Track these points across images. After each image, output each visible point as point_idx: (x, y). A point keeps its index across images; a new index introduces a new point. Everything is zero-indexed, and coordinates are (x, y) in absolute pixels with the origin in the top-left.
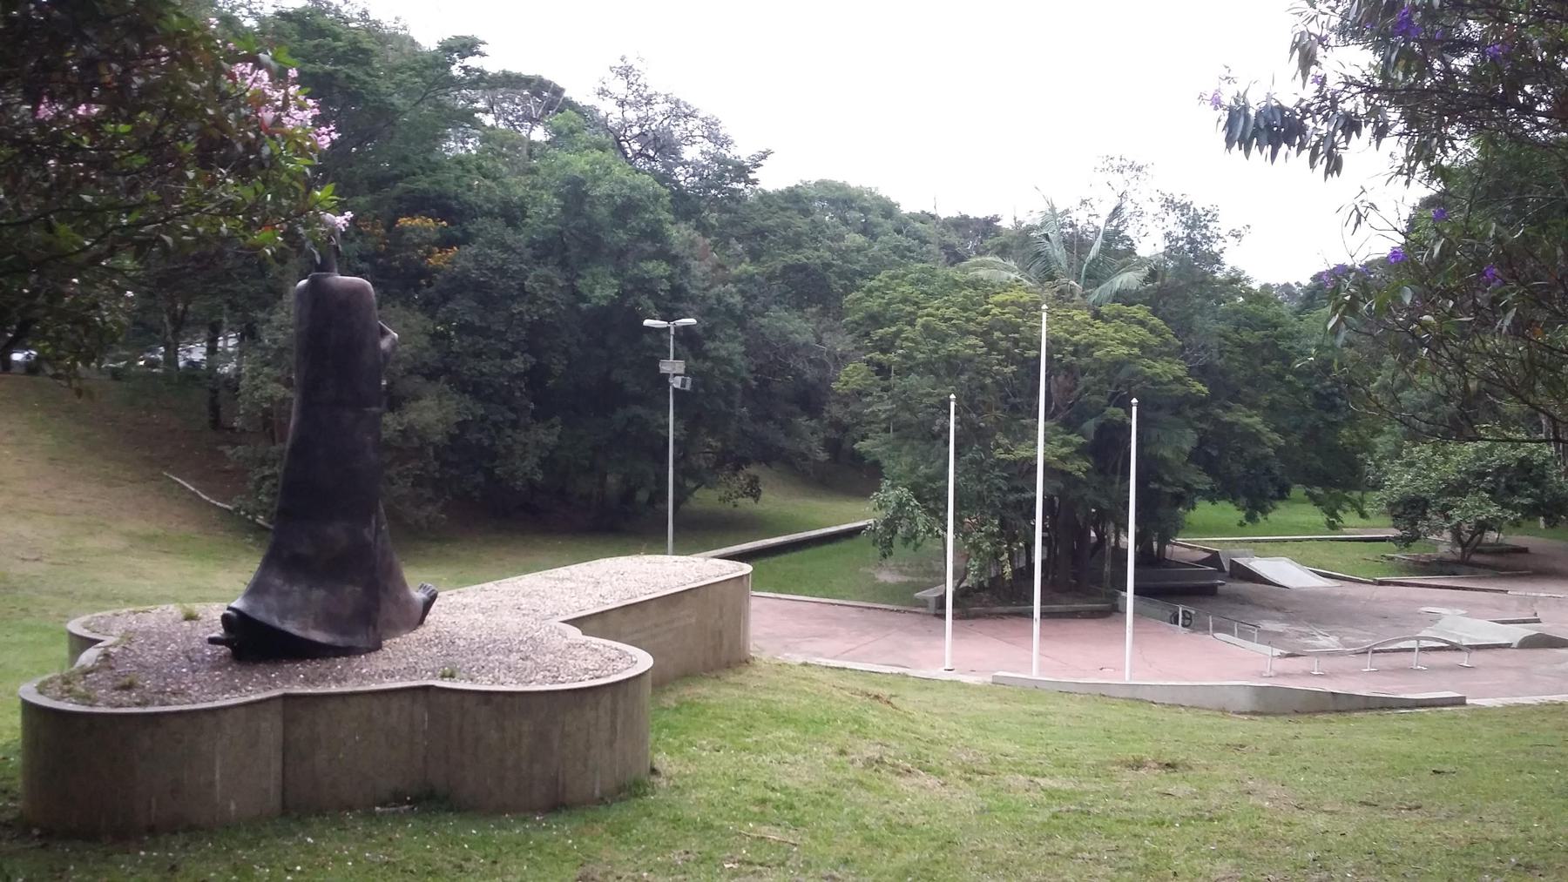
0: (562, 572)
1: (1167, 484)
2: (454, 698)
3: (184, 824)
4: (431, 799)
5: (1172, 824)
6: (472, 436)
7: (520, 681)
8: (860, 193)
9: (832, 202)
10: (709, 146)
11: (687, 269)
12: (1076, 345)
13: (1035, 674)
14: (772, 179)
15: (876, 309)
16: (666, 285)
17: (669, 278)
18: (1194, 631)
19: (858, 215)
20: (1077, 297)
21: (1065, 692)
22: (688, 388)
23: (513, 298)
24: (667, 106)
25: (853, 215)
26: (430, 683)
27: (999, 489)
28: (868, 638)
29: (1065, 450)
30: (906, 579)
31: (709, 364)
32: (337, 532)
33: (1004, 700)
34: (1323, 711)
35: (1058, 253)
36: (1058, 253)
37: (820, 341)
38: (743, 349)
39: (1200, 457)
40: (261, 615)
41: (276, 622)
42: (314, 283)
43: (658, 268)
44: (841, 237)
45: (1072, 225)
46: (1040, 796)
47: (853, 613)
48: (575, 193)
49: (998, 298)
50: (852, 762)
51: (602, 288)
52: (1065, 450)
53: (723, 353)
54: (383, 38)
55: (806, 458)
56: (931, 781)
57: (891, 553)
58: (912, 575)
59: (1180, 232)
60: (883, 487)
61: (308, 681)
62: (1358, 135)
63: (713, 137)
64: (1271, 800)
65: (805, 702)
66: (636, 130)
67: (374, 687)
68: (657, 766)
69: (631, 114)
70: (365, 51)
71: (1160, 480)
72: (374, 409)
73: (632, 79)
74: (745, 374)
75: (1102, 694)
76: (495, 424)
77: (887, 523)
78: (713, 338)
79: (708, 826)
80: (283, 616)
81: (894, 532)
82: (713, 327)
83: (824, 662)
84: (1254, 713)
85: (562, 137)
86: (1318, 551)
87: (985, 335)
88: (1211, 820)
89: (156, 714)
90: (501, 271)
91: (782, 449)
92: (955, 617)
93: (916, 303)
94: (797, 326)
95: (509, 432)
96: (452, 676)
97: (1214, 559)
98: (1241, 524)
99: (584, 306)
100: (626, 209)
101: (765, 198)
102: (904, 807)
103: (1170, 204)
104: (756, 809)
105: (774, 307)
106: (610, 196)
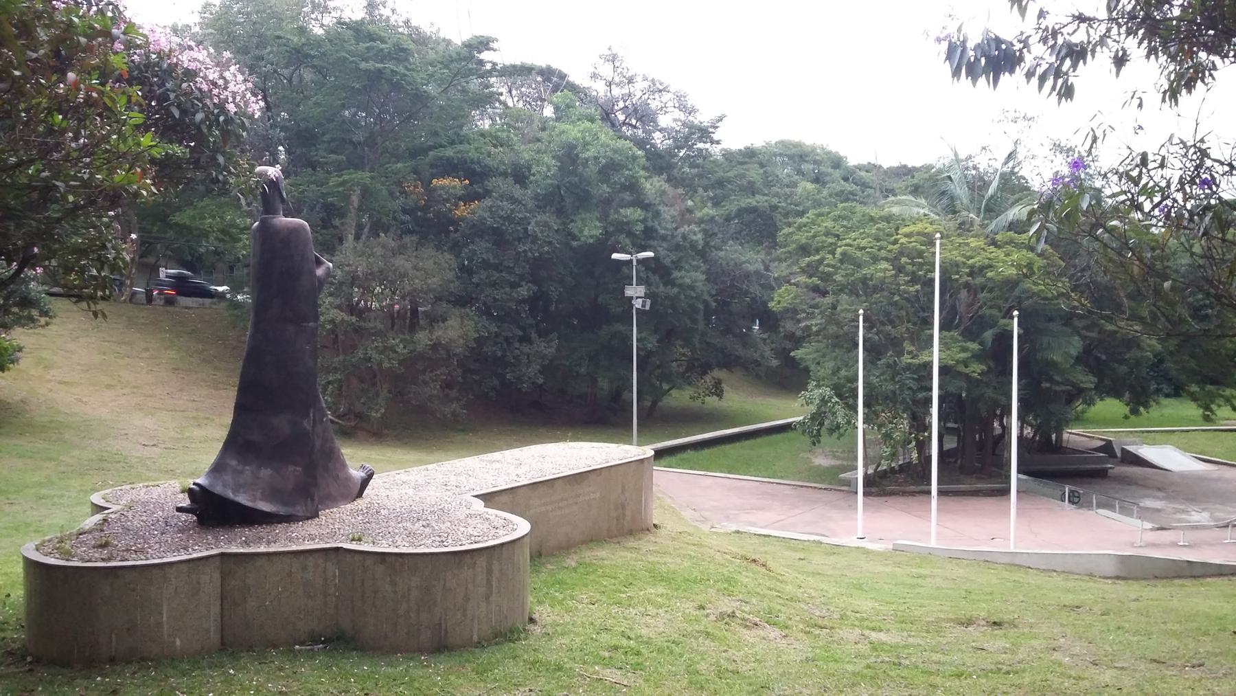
0: (497, 455)
1: (1058, 384)
2: (357, 558)
3: (139, 657)
4: (339, 640)
5: (970, 676)
6: (488, 349)
7: (412, 544)
8: (814, 150)
9: (791, 157)
10: (682, 116)
11: (657, 214)
12: (972, 267)
13: (933, 543)
14: (732, 138)
15: (804, 241)
16: (640, 227)
17: (644, 221)
18: (1081, 507)
19: (811, 167)
20: (976, 227)
21: (955, 558)
22: (647, 308)
23: (519, 240)
24: (646, 84)
25: (805, 167)
26: (340, 545)
27: (910, 388)
28: (797, 511)
29: (963, 355)
30: (838, 463)
31: (676, 290)
32: (282, 423)
33: (898, 565)
34: (1179, 577)
35: (961, 192)
36: (961, 192)
37: (767, 269)
38: (704, 277)
39: (1086, 359)
40: (218, 489)
41: (230, 495)
42: (263, 222)
43: (633, 214)
44: (794, 185)
45: (975, 168)
46: (864, 648)
47: (788, 491)
48: (570, 156)
49: (906, 230)
50: (707, 616)
51: (589, 229)
52: (963, 355)
53: (688, 281)
54: (421, 40)
55: (759, 365)
56: (773, 633)
57: (819, 442)
58: (843, 459)
59: (1066, 171)
60: (810, 387)
61: (247, 543)
62: (1085, 63)
63: (683, 107)
64: (1072, 656)
65: (686, 564)
66: (621, 104)
67: (294, 548)
68: (536, 616)
69: (616, 92)
70: (404, 50)
71: (1051, 380)
72: (311, 324)
73: (617, 64)
74: (706, 297)
75: (986, 561)
76: (507, 339)
77: (813, 417)
78: (680, 268)
79: (559, 668)
80: (236, 491)
81: (821, 424)
82: (679, 260)
83: (754, 530)
84: (1118, 578)
85: (562, 113)
86: (1202, 439)
87: (894, 261)
88: (1008, 673)
89: (115, 567)
90: (509, 218)
91: (738, 357)
92: (865, 494)
93: (837, 236)
94: (750, 258)
95: (517, 345)
96: (360, 540)
97: (1108, 447)
98: (1126, 417)
99: (575, 243)
100: (610, 168)
101: (728, 155)
102: (738, 655)
103: (1057, 147)
104: (607, 654)
105: (731, 242)
106: (596, 158)
